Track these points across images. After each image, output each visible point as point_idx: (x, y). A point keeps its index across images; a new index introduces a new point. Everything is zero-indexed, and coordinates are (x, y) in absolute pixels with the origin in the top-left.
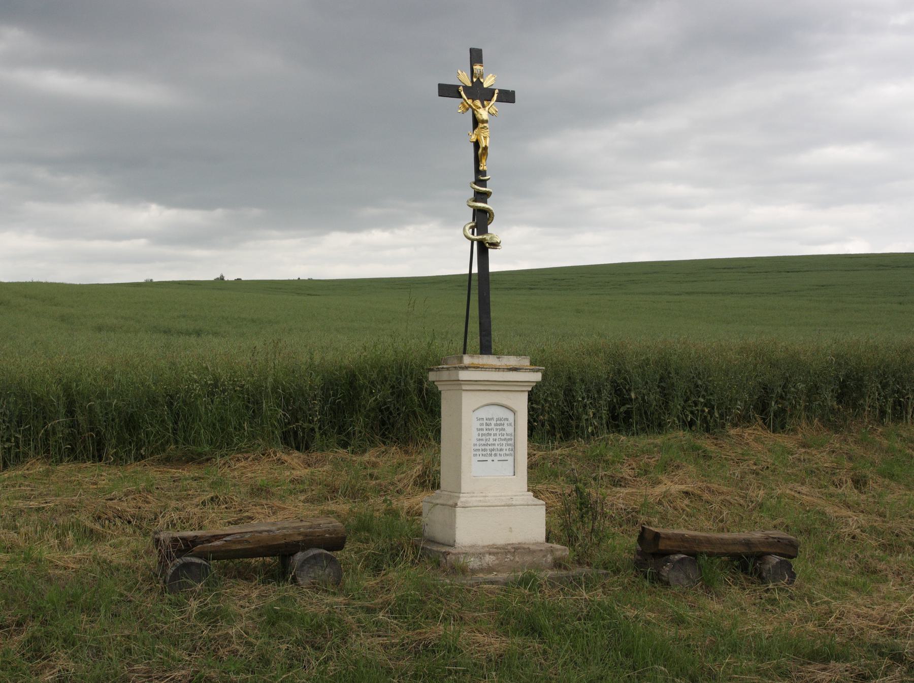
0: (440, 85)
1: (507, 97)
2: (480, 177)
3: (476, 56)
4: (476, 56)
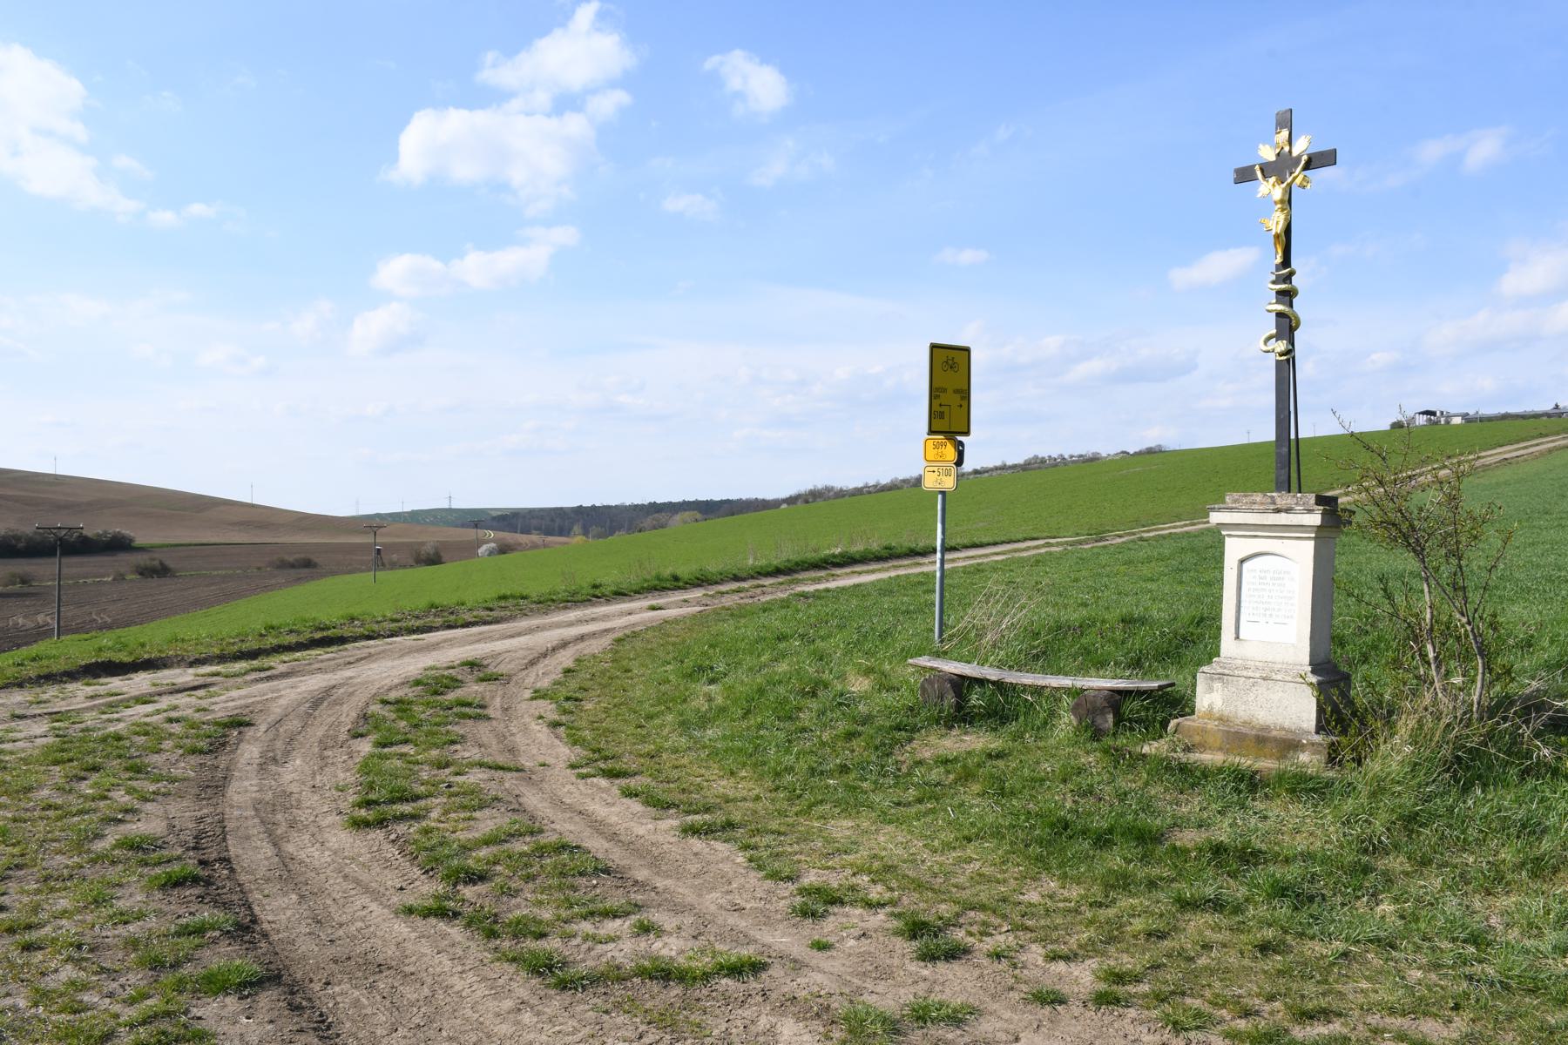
0: (934, 347)
1: (1244, 175)
3: (1285, 121)
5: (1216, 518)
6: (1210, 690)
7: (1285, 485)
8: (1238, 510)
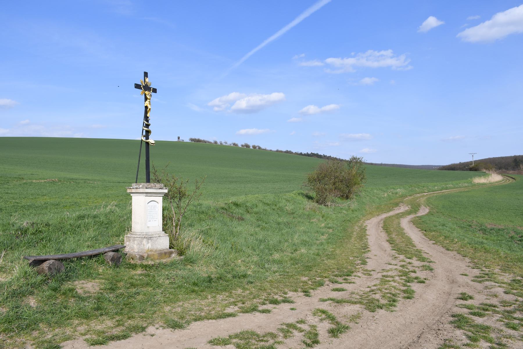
2: (146, 118)
4: (146, 74)
5: (129, 191)
6: (148, 243)
7: (148, 180)
8: (150, 188)
